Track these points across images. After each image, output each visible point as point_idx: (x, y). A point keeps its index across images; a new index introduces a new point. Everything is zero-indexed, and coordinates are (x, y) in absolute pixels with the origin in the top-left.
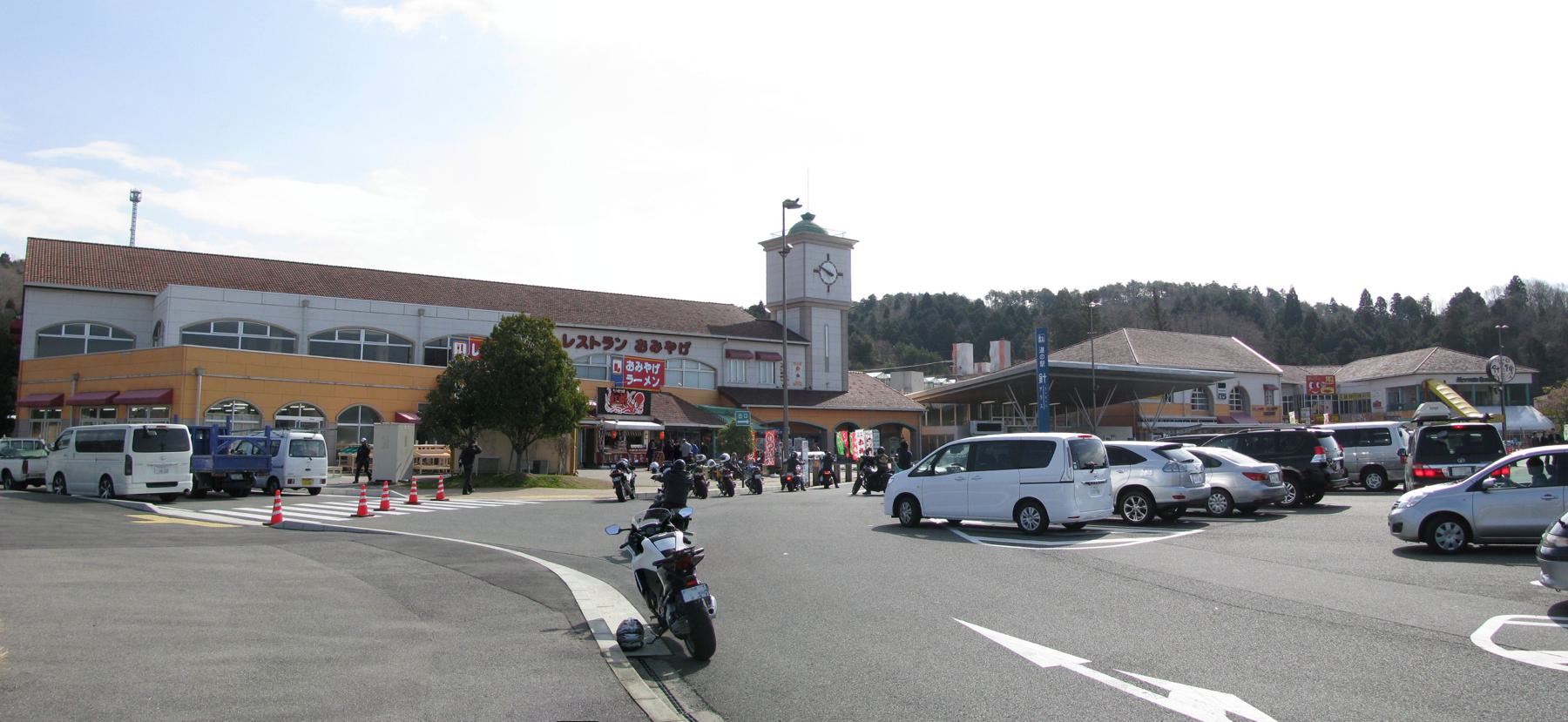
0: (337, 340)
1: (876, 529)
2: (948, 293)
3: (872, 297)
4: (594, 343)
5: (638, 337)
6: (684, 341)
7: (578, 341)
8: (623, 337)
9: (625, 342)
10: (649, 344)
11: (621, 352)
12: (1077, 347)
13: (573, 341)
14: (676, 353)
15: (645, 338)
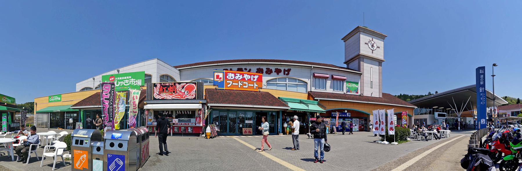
10: (265, 70)
14: (281, 75)
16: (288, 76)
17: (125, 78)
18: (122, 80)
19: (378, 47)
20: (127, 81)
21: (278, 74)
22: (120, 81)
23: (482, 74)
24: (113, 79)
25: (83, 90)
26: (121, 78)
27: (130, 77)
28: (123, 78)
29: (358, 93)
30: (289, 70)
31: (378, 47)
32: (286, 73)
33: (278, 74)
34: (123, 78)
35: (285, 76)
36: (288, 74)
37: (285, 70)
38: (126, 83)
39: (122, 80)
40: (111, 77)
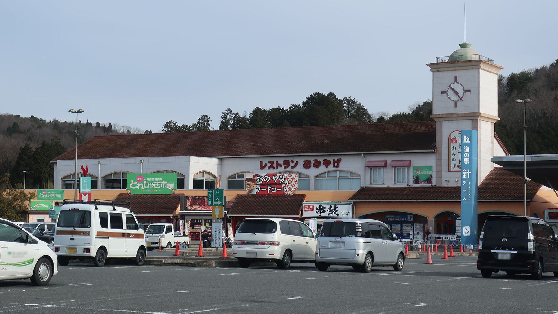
0: (237, 179)
1: (427, 65)
2: (539, 68)
3: (419, 105)
4: (278, 165)
5: (305, 159)
6: (339, 157)
7: (269, 165)
8: (295, 160)
9: (297, 162)
10: (313, 162)
11: (295, 170)
12: (138, 160)
13: (266, 165)
14: (331, 167)
15: (309, 159)
16: (338, 169)
17: (156, 179)
18: (152, 182)
19: (456, 80)
20: (158, 184)
21: (327, 167)
22: (150, 182)
23: (467, 144)
24: (141, 179)
25: (369, 161)
26: (150, 179)
27: (161, 179)
28: (153, 179)
29: (431, 182)
30: (339, 161)
31: (456, 80)
32: (336, 164)
33: (327, 167)
34: (153, 179)
35: (335, 169)
36: (337, 166)
37: (334, 161)
38: (156, 186)
39: (152, 182)
40: (139, 177)
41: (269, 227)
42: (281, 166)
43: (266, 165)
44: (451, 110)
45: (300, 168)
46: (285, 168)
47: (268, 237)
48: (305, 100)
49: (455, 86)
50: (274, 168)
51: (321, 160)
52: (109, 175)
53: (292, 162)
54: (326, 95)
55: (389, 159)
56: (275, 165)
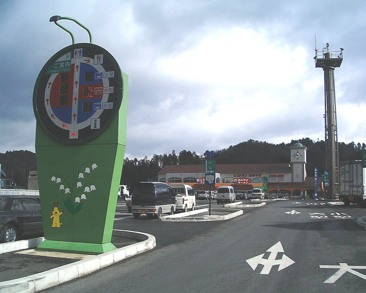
1: (174, 151)
9: (247, 175)
41: (204, 193)
42: (241, 176)
43: (236, 175)
44: (296, 161)
45: (248, 177)
46: (243, 176)
47: (205, 194)
48: (271, 143)
49: (298, 154)
50: (239, 176)
51: (255, 174)
52: (186, 178)
53: (245, 175)
54: (324, 140)
55: (277, 174)
56: (239, 175)
